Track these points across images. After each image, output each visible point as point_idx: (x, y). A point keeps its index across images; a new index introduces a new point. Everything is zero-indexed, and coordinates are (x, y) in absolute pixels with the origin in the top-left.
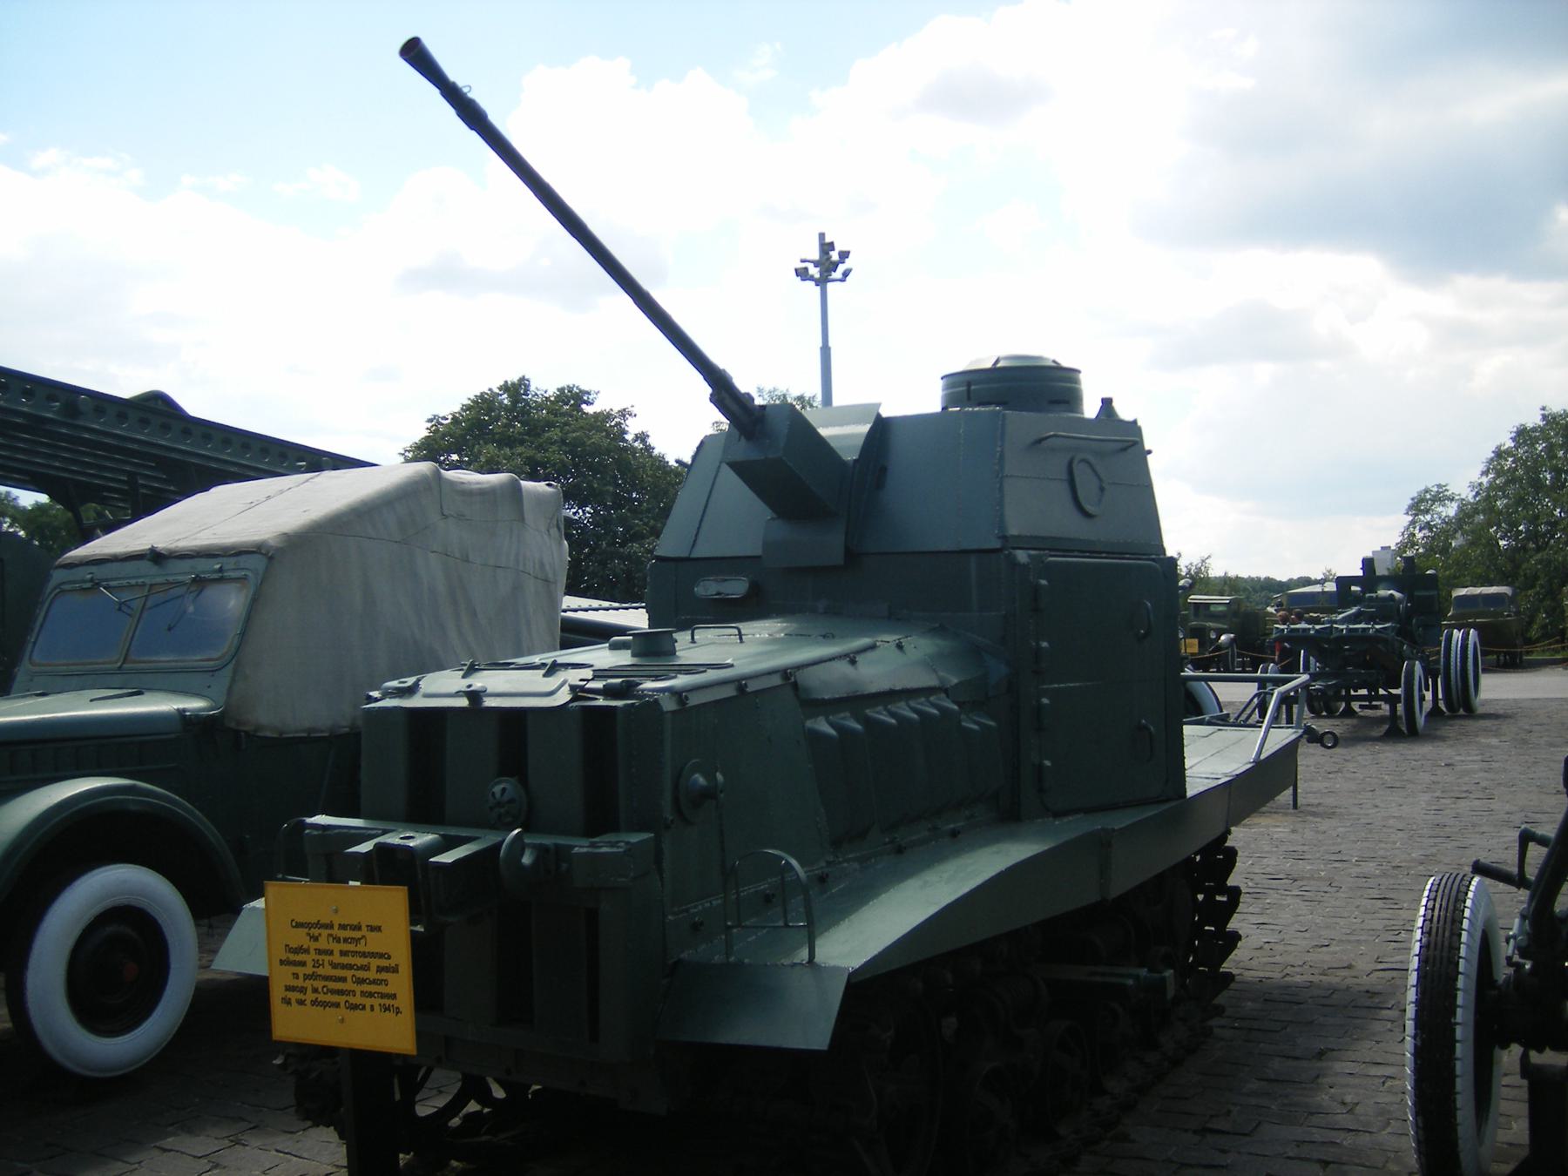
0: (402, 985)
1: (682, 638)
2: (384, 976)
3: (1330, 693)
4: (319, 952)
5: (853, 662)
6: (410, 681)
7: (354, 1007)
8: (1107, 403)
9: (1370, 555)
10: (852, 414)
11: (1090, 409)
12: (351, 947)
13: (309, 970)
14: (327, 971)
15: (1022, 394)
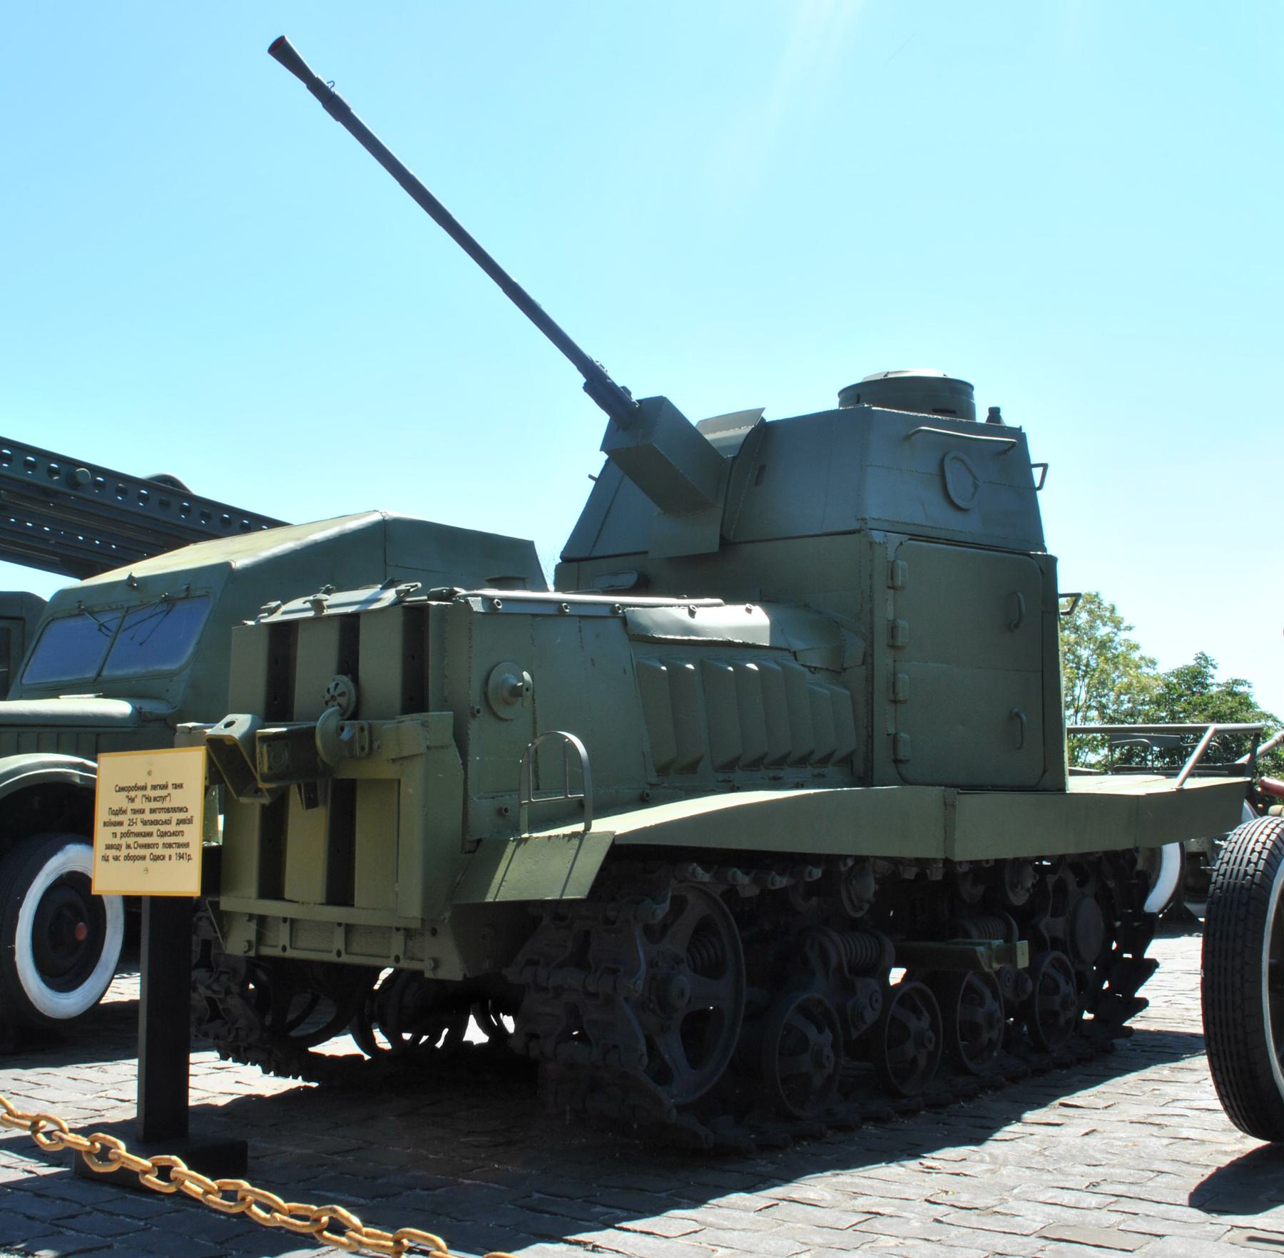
4: (135, 811)
7: (157, 858)
8: (994, 413)
11: (981, 417)
13: (124, 829)
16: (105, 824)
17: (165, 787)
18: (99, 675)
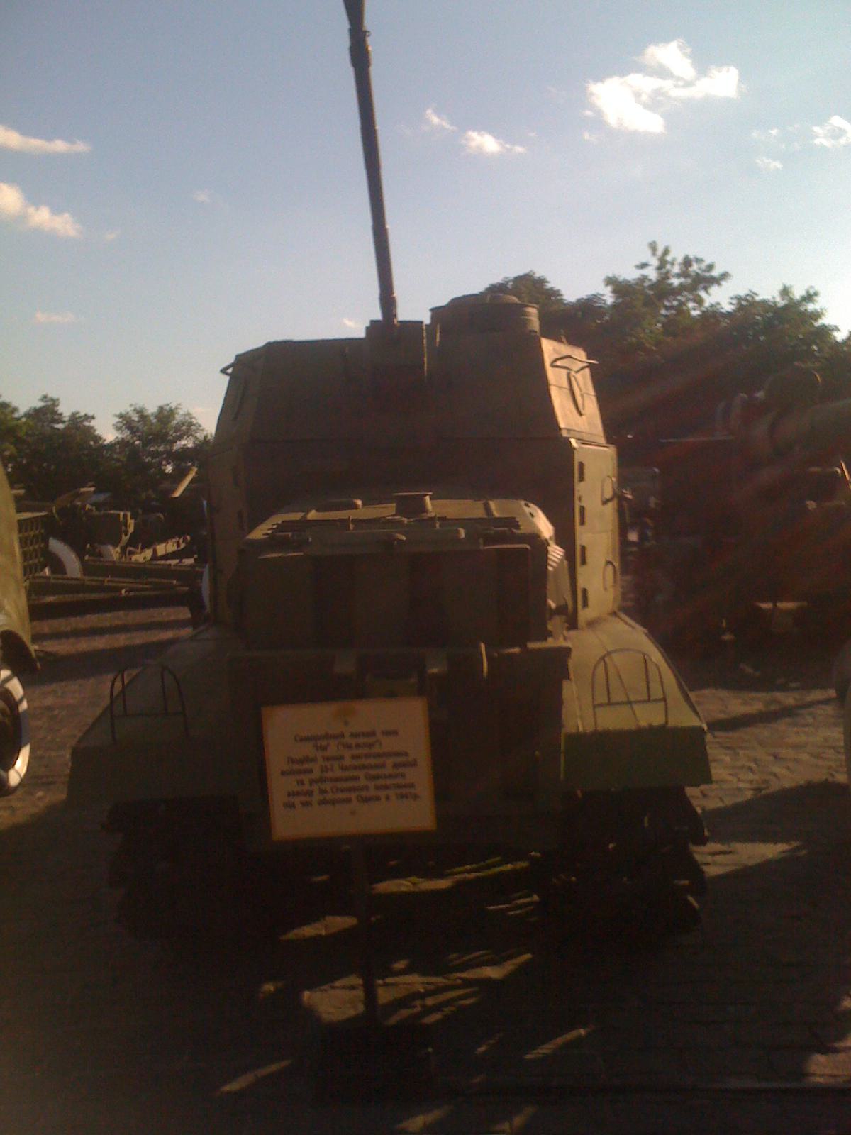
7: (367, 800)
13: (316, 774)
16: (283, 773)
17: (373, 734)
18: (123, 684)
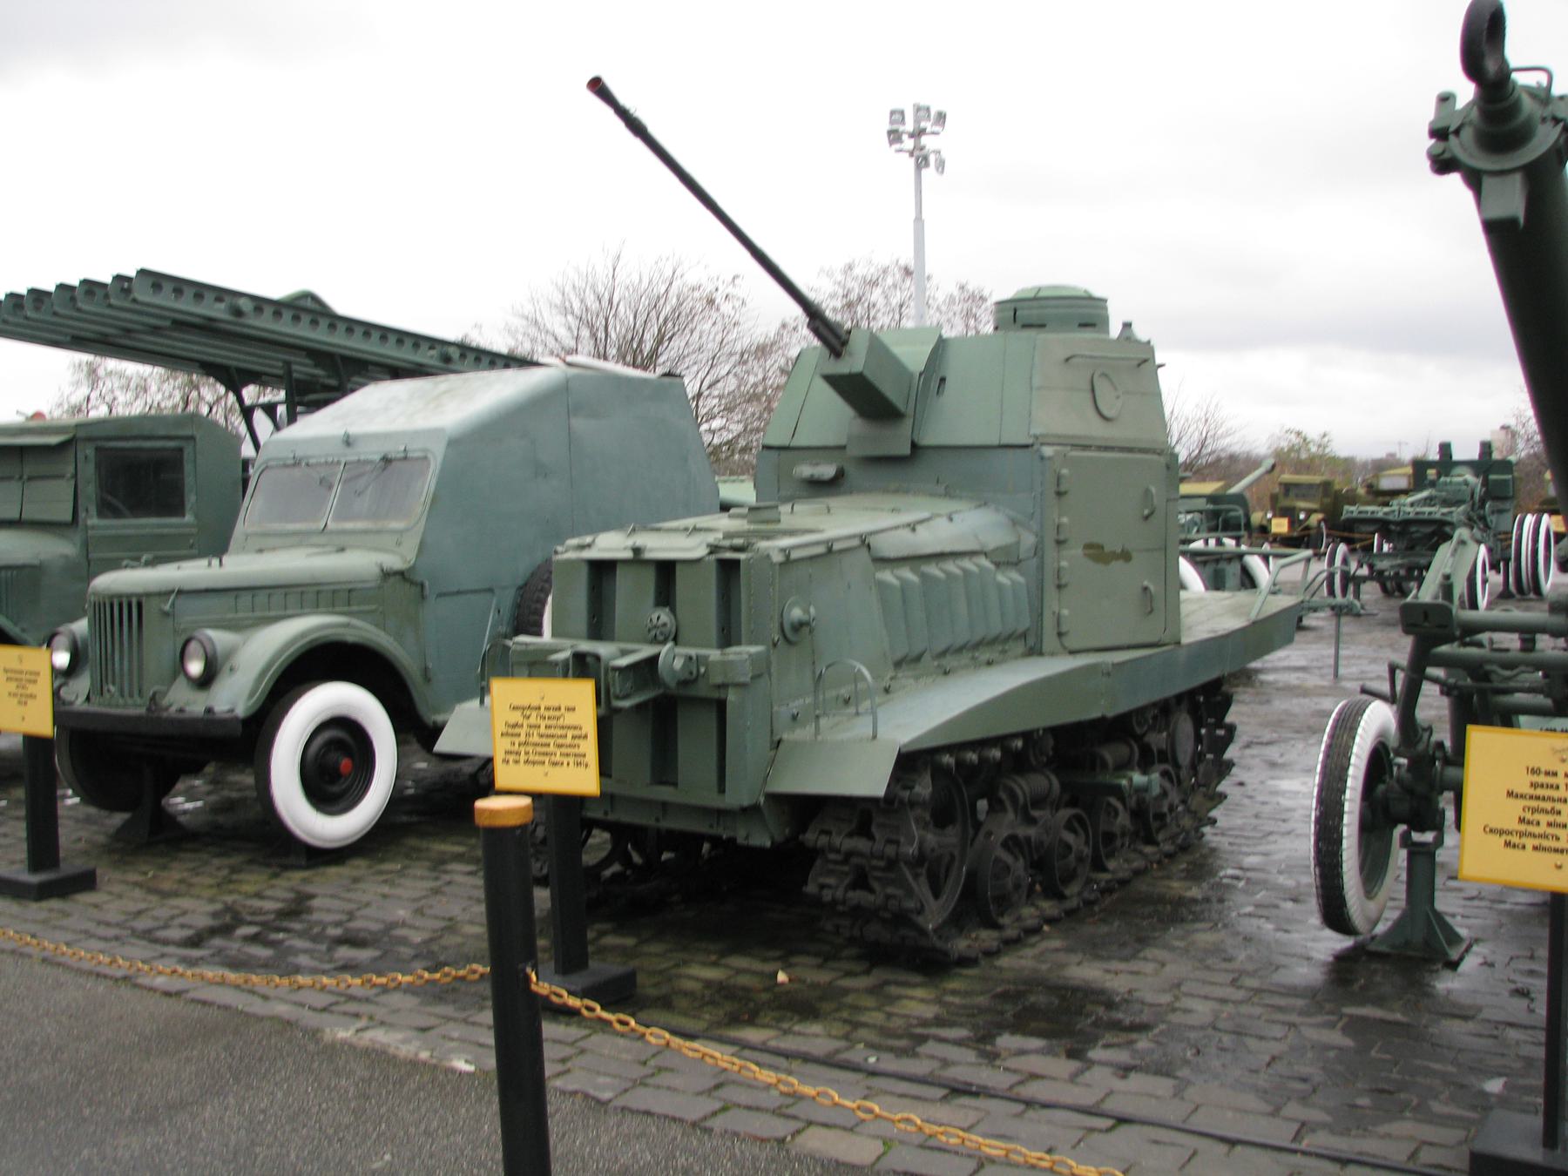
0: (590, 748)
1: (785, 509)
2: (576, 741)
3: (1402, 572)
4: (530, 726)
5: (914, 530)
6: (588, 539)
7: (555, 764)
8: (1127, 326)
9: (1487, 438)
10: (918, 332)
11: (1115, 330)
12: (553, 722)
13: (523, 738)
14: (536, 739)
15: (1052, 318)
